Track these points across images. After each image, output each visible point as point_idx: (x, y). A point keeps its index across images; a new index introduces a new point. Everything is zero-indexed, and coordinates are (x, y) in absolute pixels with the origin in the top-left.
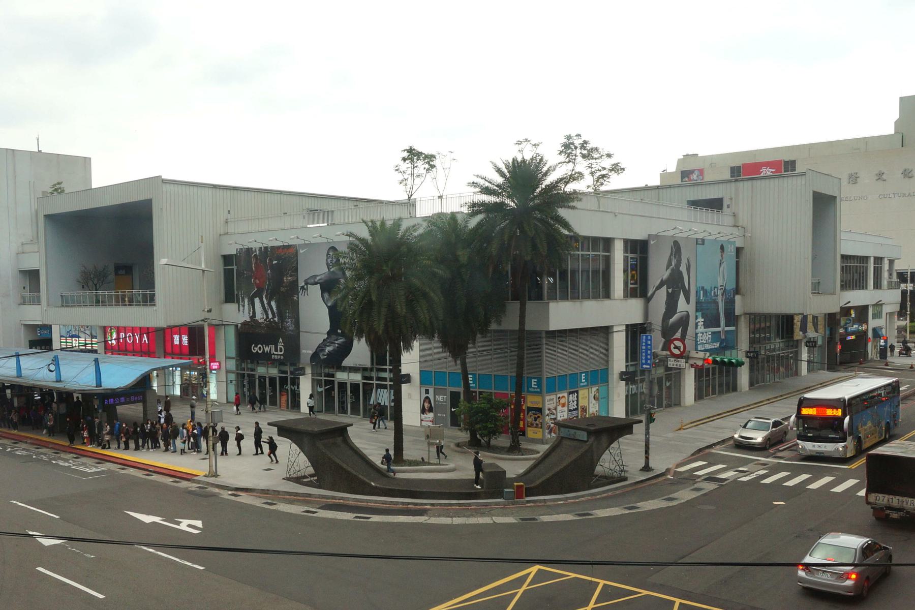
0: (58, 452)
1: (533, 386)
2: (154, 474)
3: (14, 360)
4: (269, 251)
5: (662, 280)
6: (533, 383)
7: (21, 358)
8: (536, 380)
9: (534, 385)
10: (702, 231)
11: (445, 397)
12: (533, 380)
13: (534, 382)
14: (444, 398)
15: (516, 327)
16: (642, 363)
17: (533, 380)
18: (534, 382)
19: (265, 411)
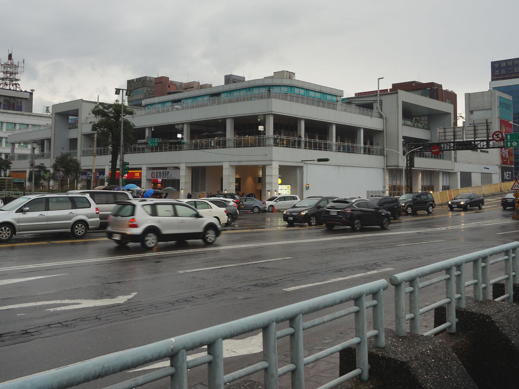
10: (474, 112)
11: (510, 173)
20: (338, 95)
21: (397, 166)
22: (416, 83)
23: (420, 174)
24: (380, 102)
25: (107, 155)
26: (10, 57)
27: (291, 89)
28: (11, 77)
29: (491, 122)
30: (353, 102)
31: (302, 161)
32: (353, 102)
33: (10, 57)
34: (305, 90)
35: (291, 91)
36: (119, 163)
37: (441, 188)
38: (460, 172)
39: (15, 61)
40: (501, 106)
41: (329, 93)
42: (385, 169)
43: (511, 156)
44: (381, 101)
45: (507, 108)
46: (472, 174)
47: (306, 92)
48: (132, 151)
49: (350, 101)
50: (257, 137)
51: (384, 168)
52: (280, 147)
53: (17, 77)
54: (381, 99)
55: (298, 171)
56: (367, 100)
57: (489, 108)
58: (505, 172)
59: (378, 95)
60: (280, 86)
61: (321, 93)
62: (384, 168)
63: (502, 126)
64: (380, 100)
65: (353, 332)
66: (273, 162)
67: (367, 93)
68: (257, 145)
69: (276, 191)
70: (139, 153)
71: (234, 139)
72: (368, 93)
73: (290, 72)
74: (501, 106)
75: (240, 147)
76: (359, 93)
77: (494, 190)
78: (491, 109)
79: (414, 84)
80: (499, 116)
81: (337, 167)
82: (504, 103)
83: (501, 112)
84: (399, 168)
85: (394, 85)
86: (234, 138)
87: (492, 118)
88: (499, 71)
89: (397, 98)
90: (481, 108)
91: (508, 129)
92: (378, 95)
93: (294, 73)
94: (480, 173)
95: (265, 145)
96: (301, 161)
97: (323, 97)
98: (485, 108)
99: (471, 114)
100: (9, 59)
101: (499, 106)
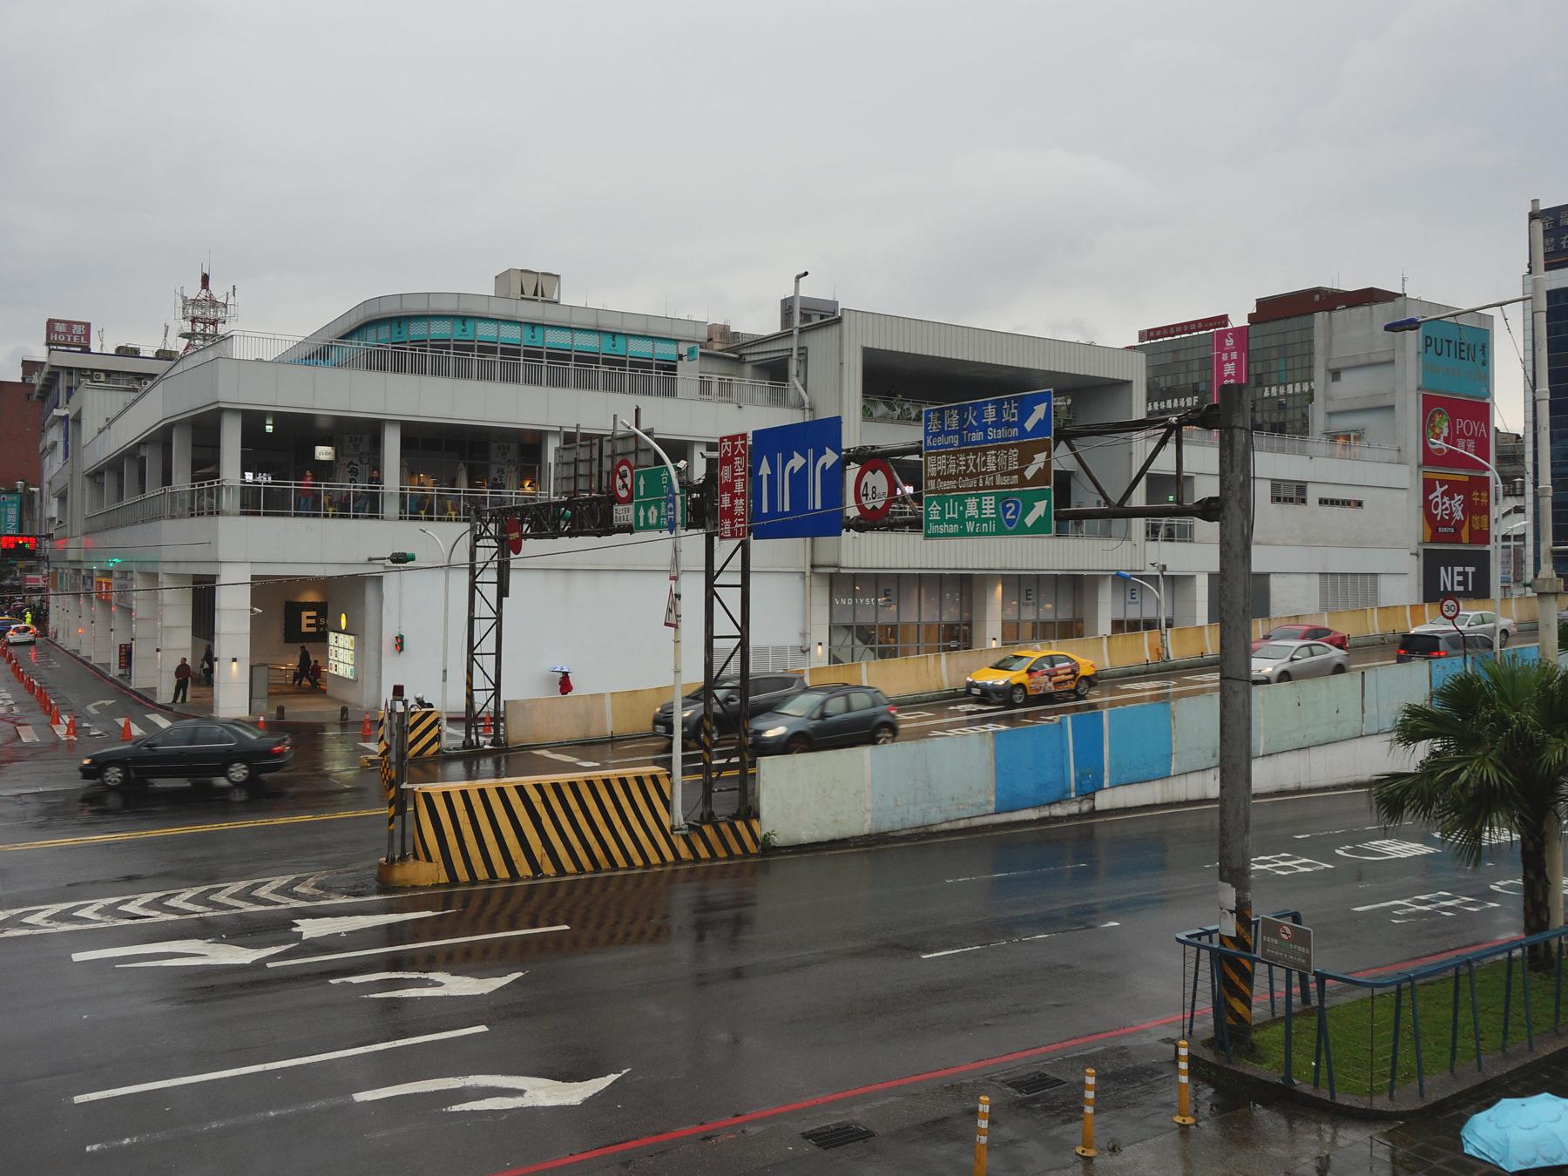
0: (721, 353)
1: (304, 629)
2: (141, 895)
3: (588, 473)
4: (1088, 1102)
5: (1211, 575)
6: (305, 621)
7: (588, 478)
8: (313, 614)
9: (308, 625)
10: (1344, 376)
11: (1471, 570)
12: (305, 614)
13: (308, 618)
14: (1464, 574)
15: (916, 620)
16: (744, 498)
17: (305, 614)
18: (308, 618)
19: (563, 384)
20: (681, 338)
21: (836, 566)
22: (1326, 292)
23: (996, 586)
24: (799, 355)
25: (1190, 541)
26: (205, 280)
27: (464, 324)
28: (208, 332)
29: (1392, 404)
30: (748, 359)
31: (370, 559)
32: (748, 359)
33: (205, 280)
34: (395, 325)
35: (399, 333)
36: (1119, 498)
37: (1104, 627)
38: (1209, 575)
39: (218, 290)
40: (1432, 349)
41: (661, 336)
42: (808, 574)
43: (1480, 514)
44: (802, 352)
45: (1463, 355)
46: (1274, 582)
47: (396, 330)
48: (445, 511)
49: (741, 355)
50: (206, 486)
51: (804, 573)
52: (326, 520)
53: (222, 329)
54: (806, 345)
55: (370, 594)
56: (764, 350)
57: (1385, 358)
58: (1442, 568)
59: (796, 332)
60: (497, 320)
61: (603, 336)
62: (804, 573)
63: (1433, 416)
64: (799, 348)
65: (1257, 986)
66: (223, 566)
67: (1172, 329)
68: (196, 512)
69: (234, 660)
70: (342, 516)
71: (193, 490)
72: (1175, 329)
73: (538, 273)
74: (1432, 349)
75: (283, 515)
76: (1149, 331)
77: (948, 677)
78: (1391, 362)
79: (1317, 297)
80: (1421, 382)
81: (559, 576)
82: (1449, 341)
83: (1427, 369)
84: (842, 571)
85: (1261, 303)
86: (194, 486)
87: (1393, 391)
88: (1552, 240)
89: (841, 338)
90: (1364, 360)
91: (1468, 424)
92: (796, 332)
93: (558, 276)
94: (1317, 578)
95: (215, 510)
96: (364, 558)
97: (614, 346)
98: (1374, 359)
99: (1333, 380)
100: (202, 288)
101: (1421, 349)
